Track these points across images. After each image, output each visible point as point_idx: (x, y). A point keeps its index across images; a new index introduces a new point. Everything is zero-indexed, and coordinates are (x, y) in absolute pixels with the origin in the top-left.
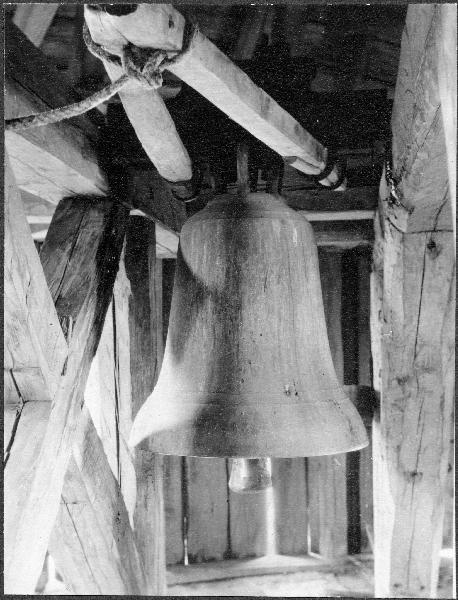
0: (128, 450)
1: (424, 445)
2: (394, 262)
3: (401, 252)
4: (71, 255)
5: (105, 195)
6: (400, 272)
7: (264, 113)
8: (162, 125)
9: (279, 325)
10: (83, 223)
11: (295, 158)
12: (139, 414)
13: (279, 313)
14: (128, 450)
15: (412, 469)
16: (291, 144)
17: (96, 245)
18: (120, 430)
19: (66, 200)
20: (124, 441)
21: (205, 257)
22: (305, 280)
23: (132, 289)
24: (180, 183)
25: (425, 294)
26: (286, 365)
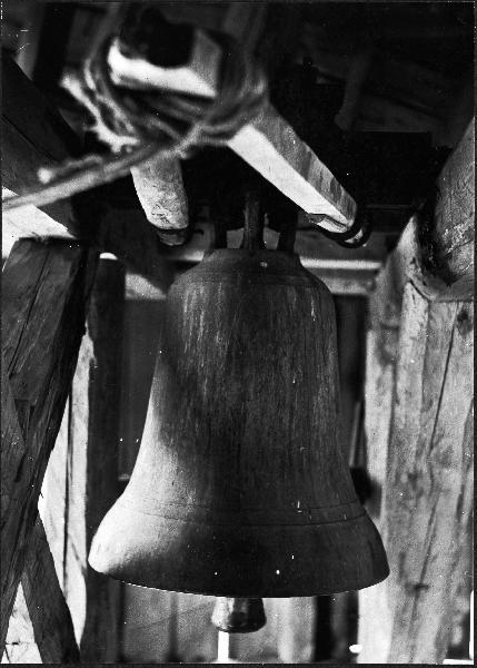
0: (77, 558)
1: (433, 553)
2: (415, 334)
3: (425, 324)
4: (29, 316)
5: (60, 230)
6: (422, 349)
7: (305, 171)
8: (171, 177)
9: (291, 421)
10: (45, 272)
11: (323, 216)
12: (101, 529)
13: (292, 408)
14: (77, 558)
15: (415, 578)
16: (325, 202)
17: (62, 303)
18: (70, 532)
19: (23, 240)
20: (73, 545)
21: (202, 330)
22: (322, 364)
23: (95, 352)
24: (172, 231)
25: (450, 374)
26: (297, 474)
